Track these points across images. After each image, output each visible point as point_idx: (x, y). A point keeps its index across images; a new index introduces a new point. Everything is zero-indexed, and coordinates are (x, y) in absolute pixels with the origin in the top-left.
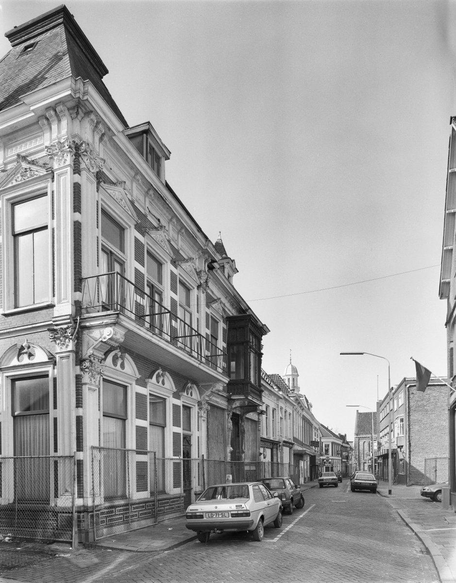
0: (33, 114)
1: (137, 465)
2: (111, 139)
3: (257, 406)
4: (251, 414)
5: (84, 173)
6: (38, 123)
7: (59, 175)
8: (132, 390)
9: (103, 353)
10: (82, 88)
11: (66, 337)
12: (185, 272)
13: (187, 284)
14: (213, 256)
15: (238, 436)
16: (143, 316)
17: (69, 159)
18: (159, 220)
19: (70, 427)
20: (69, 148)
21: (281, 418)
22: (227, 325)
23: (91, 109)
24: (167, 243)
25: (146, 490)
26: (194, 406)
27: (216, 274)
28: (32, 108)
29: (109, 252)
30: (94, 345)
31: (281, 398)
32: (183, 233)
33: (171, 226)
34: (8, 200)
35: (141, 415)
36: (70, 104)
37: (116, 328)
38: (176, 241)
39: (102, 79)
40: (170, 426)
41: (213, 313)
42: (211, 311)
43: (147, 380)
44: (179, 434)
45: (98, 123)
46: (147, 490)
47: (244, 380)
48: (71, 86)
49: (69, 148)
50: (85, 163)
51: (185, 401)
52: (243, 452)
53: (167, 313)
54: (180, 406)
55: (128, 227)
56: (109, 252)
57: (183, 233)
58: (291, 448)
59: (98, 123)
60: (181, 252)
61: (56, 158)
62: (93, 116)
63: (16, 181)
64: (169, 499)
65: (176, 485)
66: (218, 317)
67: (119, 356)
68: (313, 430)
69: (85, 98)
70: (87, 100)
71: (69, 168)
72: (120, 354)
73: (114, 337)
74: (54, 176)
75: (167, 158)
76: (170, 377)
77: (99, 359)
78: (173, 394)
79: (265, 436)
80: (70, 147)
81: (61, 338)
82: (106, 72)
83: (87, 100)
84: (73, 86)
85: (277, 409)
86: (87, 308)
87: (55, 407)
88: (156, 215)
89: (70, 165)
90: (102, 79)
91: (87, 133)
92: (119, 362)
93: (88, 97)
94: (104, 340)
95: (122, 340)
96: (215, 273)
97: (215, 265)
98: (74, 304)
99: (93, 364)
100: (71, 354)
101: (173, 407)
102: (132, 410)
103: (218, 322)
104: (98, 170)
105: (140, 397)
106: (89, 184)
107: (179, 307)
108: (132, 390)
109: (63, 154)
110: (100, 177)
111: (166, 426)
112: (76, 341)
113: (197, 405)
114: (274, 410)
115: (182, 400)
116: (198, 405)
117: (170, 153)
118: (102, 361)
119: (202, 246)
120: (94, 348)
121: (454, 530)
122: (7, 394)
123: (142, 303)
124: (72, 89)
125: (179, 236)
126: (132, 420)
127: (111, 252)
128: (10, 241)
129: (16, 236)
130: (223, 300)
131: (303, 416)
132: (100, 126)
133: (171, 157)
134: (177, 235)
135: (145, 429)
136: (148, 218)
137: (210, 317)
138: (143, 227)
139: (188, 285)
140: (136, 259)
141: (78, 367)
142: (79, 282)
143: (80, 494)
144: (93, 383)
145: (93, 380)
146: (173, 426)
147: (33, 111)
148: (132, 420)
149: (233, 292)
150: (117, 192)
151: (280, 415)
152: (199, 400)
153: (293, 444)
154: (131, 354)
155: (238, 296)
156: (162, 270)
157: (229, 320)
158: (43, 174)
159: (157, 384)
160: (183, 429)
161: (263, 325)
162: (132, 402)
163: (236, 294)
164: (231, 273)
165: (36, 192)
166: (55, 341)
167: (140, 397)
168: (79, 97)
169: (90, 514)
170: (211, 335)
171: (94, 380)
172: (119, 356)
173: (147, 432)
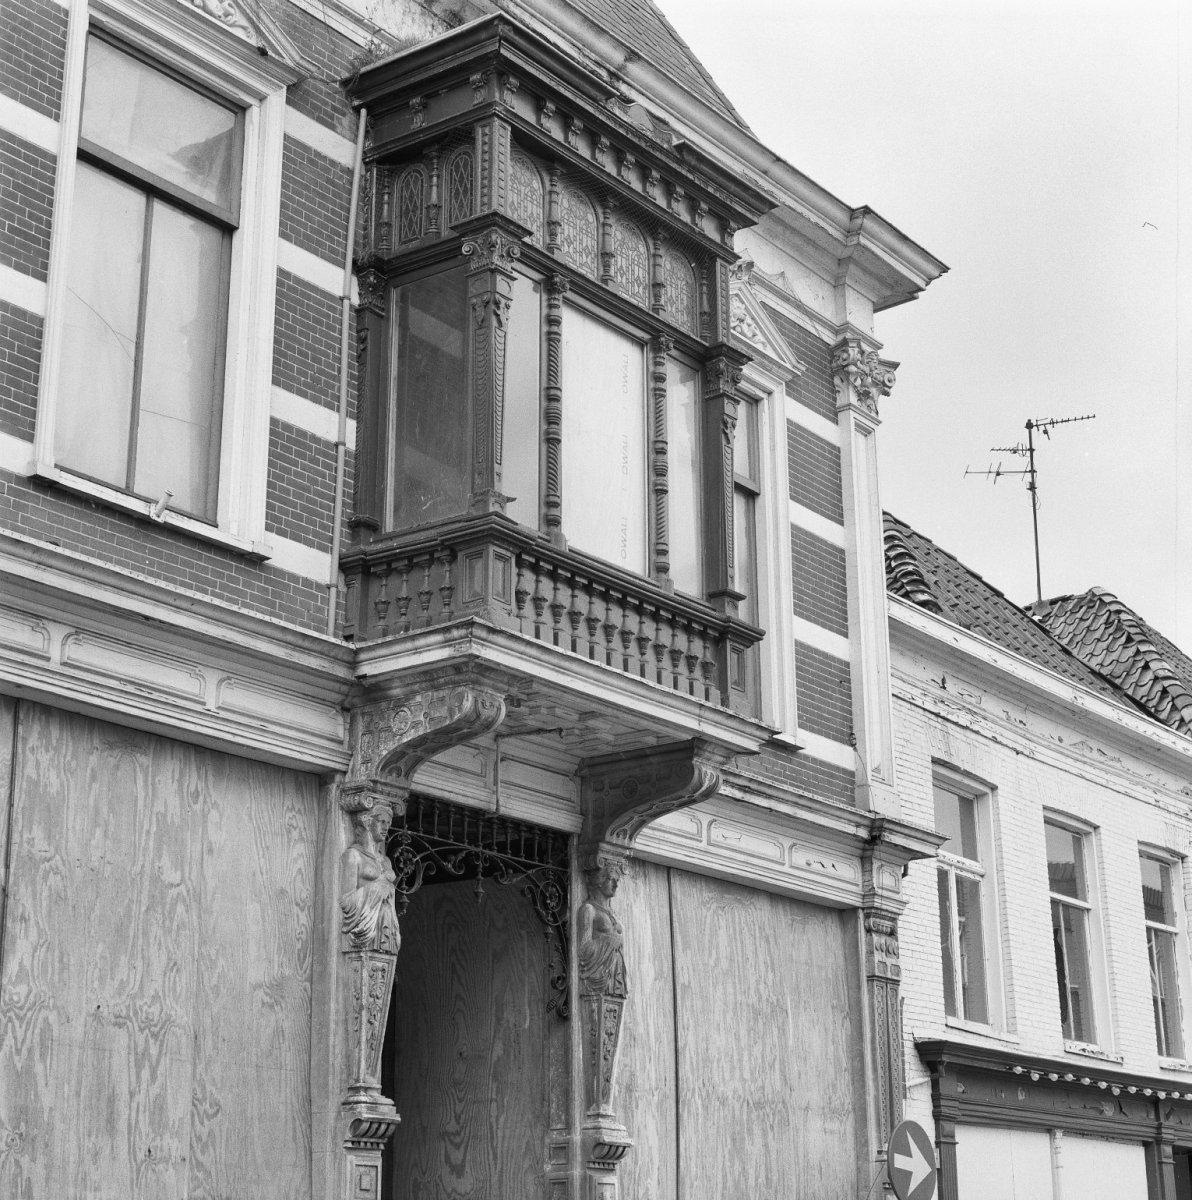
15: (564, 1017)
140: (800, 492)
161: (852, 213)
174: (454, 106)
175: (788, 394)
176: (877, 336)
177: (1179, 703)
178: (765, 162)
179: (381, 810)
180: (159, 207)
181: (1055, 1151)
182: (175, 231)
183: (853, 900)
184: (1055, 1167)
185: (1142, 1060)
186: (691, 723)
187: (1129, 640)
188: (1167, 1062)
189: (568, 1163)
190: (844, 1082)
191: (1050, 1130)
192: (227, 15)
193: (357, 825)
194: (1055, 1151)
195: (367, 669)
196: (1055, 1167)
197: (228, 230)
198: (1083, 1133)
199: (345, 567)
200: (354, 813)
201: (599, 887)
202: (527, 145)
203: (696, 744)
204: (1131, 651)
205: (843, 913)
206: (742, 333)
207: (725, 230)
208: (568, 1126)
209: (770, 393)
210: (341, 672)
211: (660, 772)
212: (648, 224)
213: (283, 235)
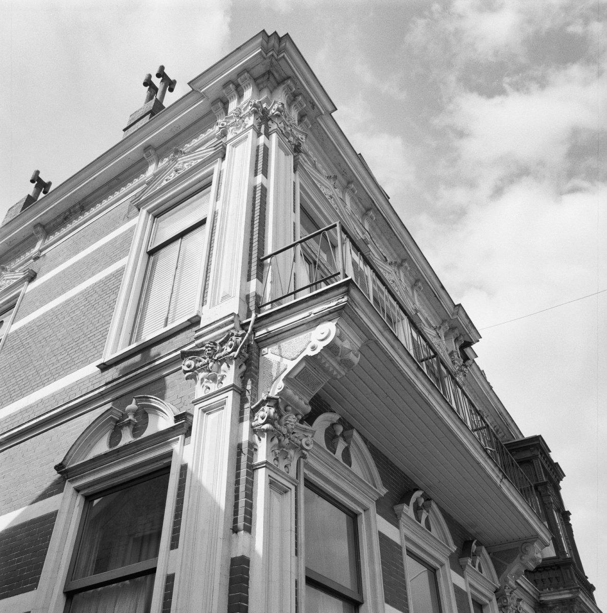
2: (314, 122)
7: (233, 146)
9: (307, 400)
10: (277, 45)
11: (221, 361)
23: (290, 73)
32: (420, 288)
43: (397, 508)
47: (558, 557)
56: (311, 261)
57: (420, 288)
67: (339, 434)
70: (283, 57)
71: (230, 394)
74: (225, 155)
83: (283, 57)
84: (265, 43)
87: (174, 544)
89: (233, 387)
92: (341, 446)
107: (408, 562)
112: (244, 367)
119: (450, 315)
120: (286, 379)
124: (262, 47)
126: (375, 604)
144: (281, 467)
152: (498, 585)
155: (504, 414)
163: (503, 411)
171: (286, 462)
172: (339, 434)
195: (543, 599)
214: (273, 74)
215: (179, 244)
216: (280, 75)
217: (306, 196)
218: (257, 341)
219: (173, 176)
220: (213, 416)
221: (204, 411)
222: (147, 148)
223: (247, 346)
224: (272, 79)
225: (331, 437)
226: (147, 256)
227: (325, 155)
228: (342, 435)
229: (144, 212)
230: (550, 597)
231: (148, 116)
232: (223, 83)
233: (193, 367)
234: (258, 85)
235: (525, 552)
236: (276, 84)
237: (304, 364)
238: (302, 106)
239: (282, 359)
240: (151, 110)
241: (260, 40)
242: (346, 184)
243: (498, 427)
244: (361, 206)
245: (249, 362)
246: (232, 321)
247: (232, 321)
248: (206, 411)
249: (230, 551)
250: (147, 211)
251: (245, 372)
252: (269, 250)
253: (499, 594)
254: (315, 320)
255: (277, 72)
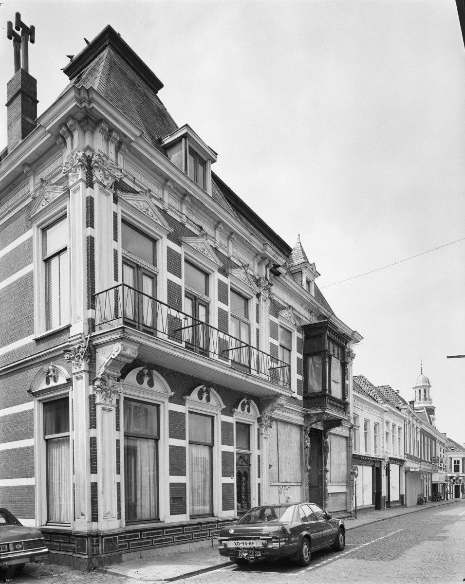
0: (49, 135)
1: (170, 489)
2: (130, 148)
3: (341, 420)
4: (337, 428)
5: (96, 186)
6: (56, 144)
7: (74, 192)
8: (164, 409)
10: (86, 97)
12: (238, 278)
13: (243, 293)
14: (275, 260)
15: (322, 454)
16: (179, 330)
17: (81, 174)
18: (201, 228)
19: (103, 454)
20: (79, 161)
21: (387, 433)
22: (303, 335)
24: (212, 251)
25: (185, 513)
26: (451, 458)
27: (284, 280)
28: (47, 128)
29: (134, 266)
30: (106, 363)
31: (386, 411)
33: (218, 233)
34: (38, 226)
35: (227, 441)
36: (80, 116)
37: (123, 343)
38: (226, 249)
39: (157, 94)
40: (218, 445)
41: (281, 321)
42: (280, 320)
43: (184, 397)
44: (231, 454)
45: (111, 131)
46: (185, 513)
48: (75, 97)
49: (79, 161)
50: (98, 175)
51: (238, 417)
52: (326, 471)
53: (200, 324)
54: (233, 424)
55: (159, 238)
56: (134, 266)
58: (400, 466)
59: (111, 131)
60: (232, 259)
61: (70, 174)
62: (103, 125)
63: (42, 205)
64: (217, 522)
65: (227, 506)
66: (290, 326)
67: (146, 373)
68: (438, 444)
69: (91, 106)
70: (93, 107)
72: (146, 371)
73: (123, 352)
75: (214, 161)
76: (217, 394)
77: (115, 378)
78: (222, 410)
79: (362, 453)
80: (80, 161)
81: (75, 358)
82: (160, 86)
83: (93, 107)
84: (77, 95)
85: (380, 423)
86: (99, 325)
88: (198, 222)
90: (157, 94)
91: (99, 144)
93: (93, 104)
94: (113, 357)
95: (135, 356)
96: (282, 278)
97: (281, 270)
98: (87, 322)
99: (107, 383)
100: (84, 373)
101: (169, 413)
102: (164, 430)
103: (291, 333)
104: (114, 181)
105: (226, 426)
106: (104, 197)
108: (218, 420)
109: (76, 170)
110: (119, 186)
111: (160, 439)
113: (256, 422)
114: (376, 425)
115: (235, 416)
116: (258, 422)
117: (217, 154)
118: (120, 380)
121: (458, 518)
122: (386, 487)
123: (178, 317)
125: (230, 242)
126: (164, 439)
127: (137, 265)
128: (40, 267)
129: (47, 261)
130: (296, 306)
131: (422, 430)
132: (114, 134)
133: (218, 159)
134: (227, 242)
135: (182, 449)
136: (186, 226)
137: (279, 326)
138: (178, 233)
139: (245, 294)
140: (170, 270)
141: (91, 387)
142: (92, 300)
143: (94, 518)
144: (108, 402)
145: (108, 400)
146: (222, 444)
147: (49, 131)
148: (164, 439)
149: (308, 298)
150: (139, 202)
151: (385, 430)
153: (403, 461)
154: (162, 370)
156: (208, 281)
157: (307, 329)
158: (61, 194)
159: (199, 401)
160: (237, 448)
161: (353, 332)
162: (164, 418)
164: (311, 278)
165: (59, 214)
166: (71, 362)
167: (226, 426)
168: (85, 107)
169: (103, 538)
170: (280, 345)
172: (146, 373)
173: (185, 452)
174: (319, 332)
175: (167, 238)
176: (353, 350)
177: (377, 397)
178: (344, 326)
179: (308, 430)
180: (284, 349)
181: (363, 468)
182: (286, 352)
183: (348, 436)
184: (363, 470)
185: (373, 455)
186: (342, 417)
187: (368, 385)
188: (366, 453)
189: (322, 473)
190: (346, 461)
191: (362, 465)
192: (152, 216)
193: (305, 432)
194: (363, 468)
195: (308, 413)
196: (363, 470)
197: (290, 351)
198: (366, 465)
199: (304, 398)
200: (305, 431)
201: (326, 437)
202: (329, 338)
203: (279, 395)
204: (368, 387)
205: (346, 438)
206: (204, 254)
207: (346, 344)
208: (322, 468)
209: (161, 238)
210: (305, 413)
211: (338, 423)
212: (338, 345)
213: (168, 271)
214: (90, 118)
215: (68, 223)
216: (95, 118)
217: (38, 414)
218: (94, 346)
219: (44, 204)
220: (80, 381)
221: (77, 378)
222: (24, 164)
223: (89, 349)
224: (90, 122)
225: (140, 379)
226: (44, 263)
227: (145, 166)
228: (147, 374)
229: (35, 226)
230: (311, 412)
231: (20, 96)
232: (58, 124)
233: (69, 358)
234: (82, 127)
235: (275, 401)
236: (94, 126)
237: (111, 361)
238: (116, 140)
239: (104, 357)
240: (20, 90)
241: (72, 94)
242: (164, 182)
243: (311, 309)
244: (179, 194)
245: (90, 354)
246: (81, 338)
247: (81, 338)
248: (77, 378)
249: (89, 435)
250: (37, 226)
251: (89, 362)
252: (97, 292)
253: (259, 420)
254: (113, 341)
255: (93, 116)
